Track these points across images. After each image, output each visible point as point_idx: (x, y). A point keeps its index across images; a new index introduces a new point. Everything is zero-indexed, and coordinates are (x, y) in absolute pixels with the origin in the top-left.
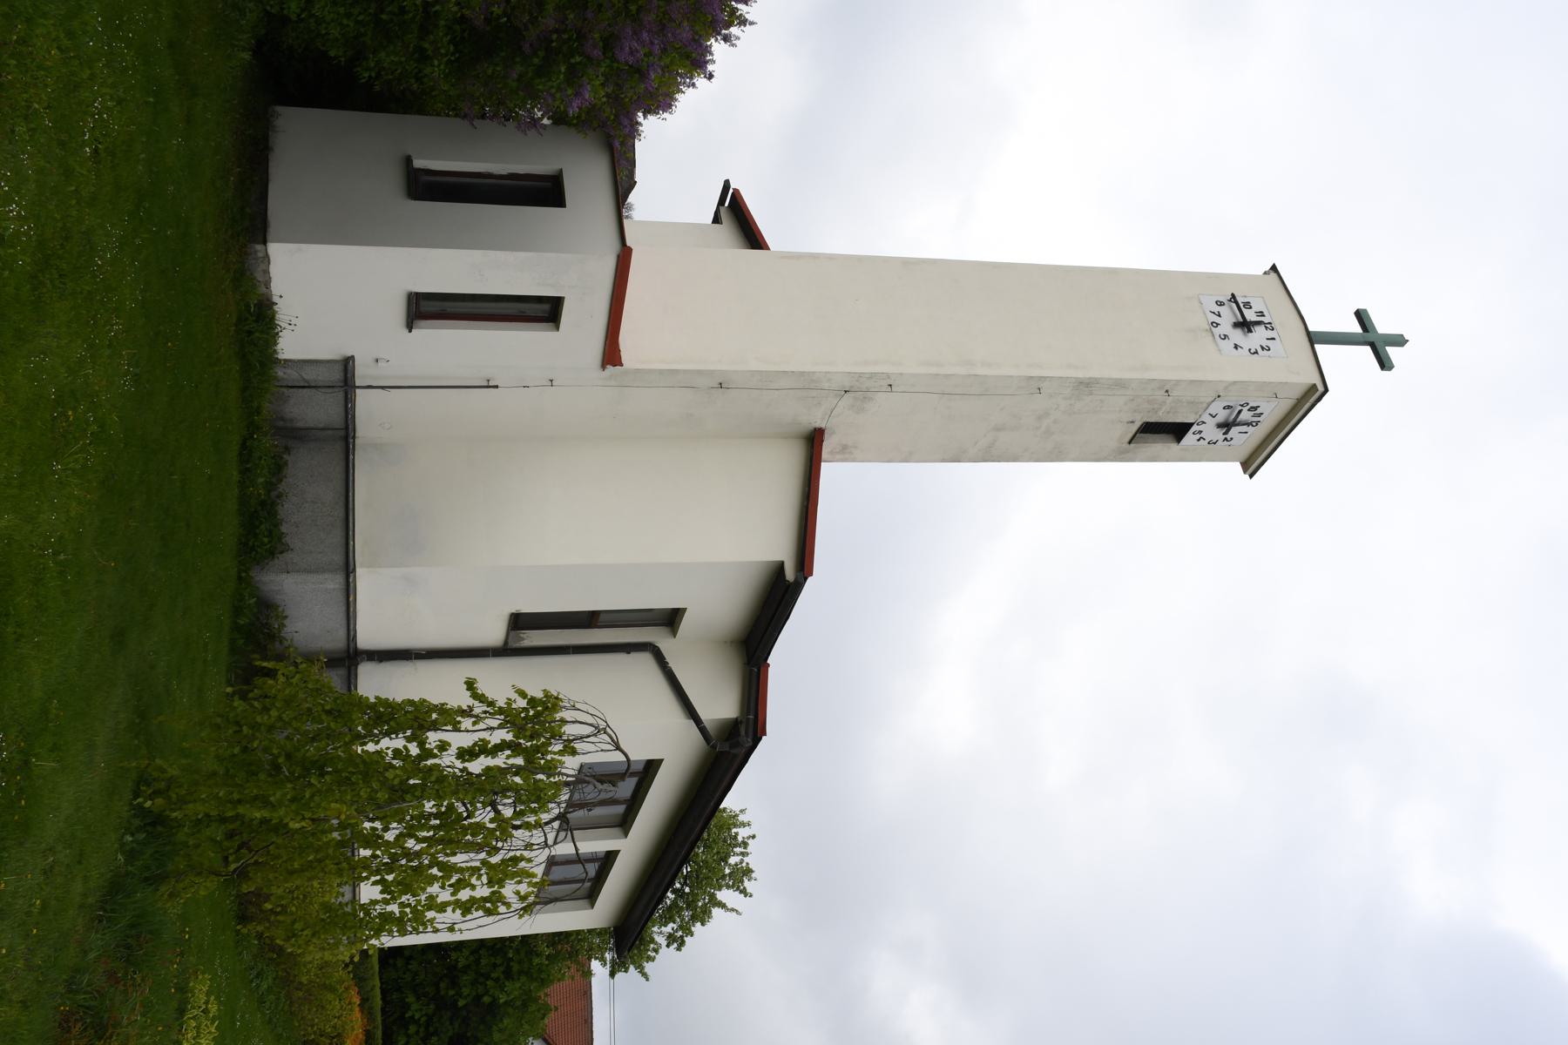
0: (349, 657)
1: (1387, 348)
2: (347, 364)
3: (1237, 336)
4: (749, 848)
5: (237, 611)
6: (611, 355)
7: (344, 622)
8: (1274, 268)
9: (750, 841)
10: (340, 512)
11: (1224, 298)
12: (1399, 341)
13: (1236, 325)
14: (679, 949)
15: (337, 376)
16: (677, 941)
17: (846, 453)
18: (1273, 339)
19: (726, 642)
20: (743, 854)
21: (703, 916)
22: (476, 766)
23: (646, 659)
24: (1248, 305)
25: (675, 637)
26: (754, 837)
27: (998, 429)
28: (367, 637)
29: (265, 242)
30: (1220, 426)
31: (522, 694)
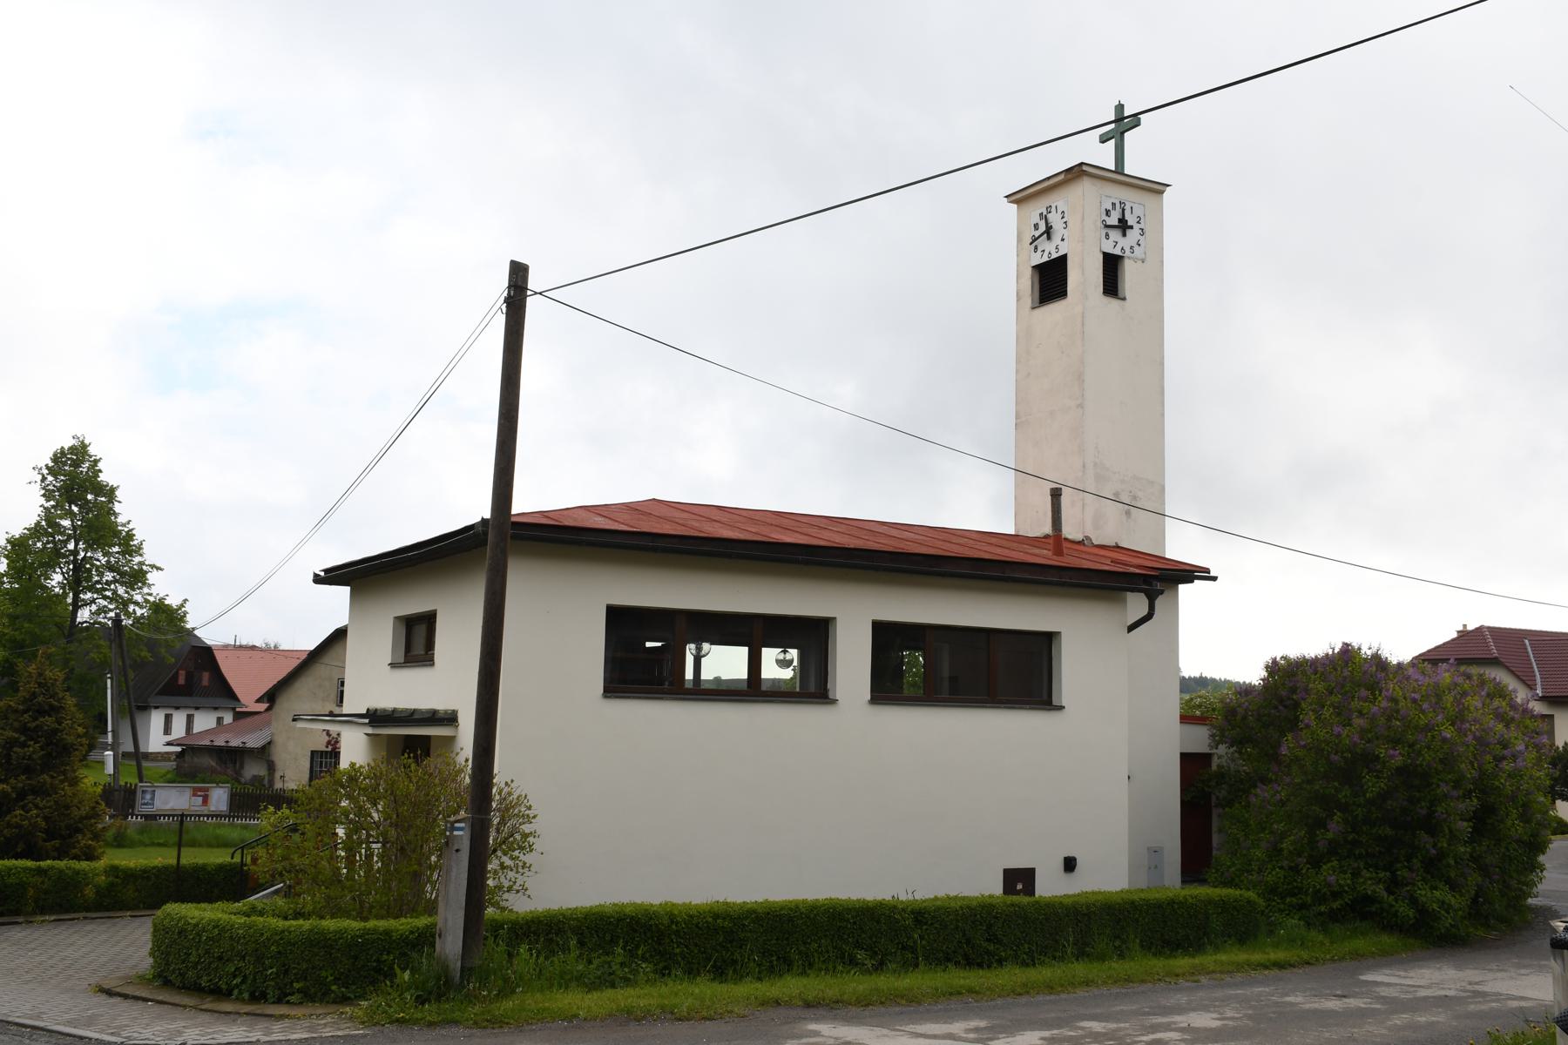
13: (1049, 238)
30: (1124, 235)
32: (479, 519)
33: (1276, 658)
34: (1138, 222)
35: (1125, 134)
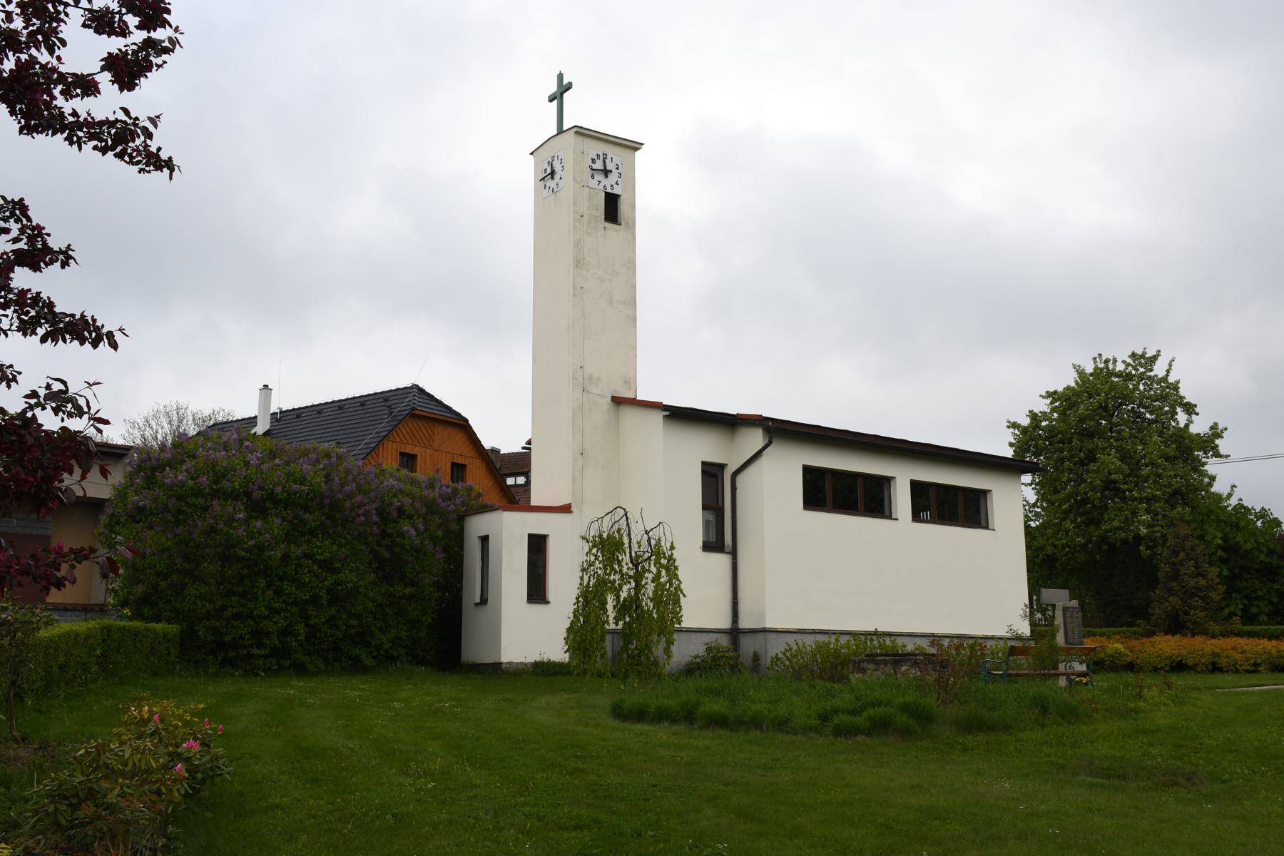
1: (564, 84)
3: (557, 177)
6: (566, 509)
7: (705, 634)
8: (532, 154)
12: (560, 76)
13: (552, 178)
17: (631, 382)
23: (739, 478)
27: (611, 302)
29: (501, 663)
30: (606, 177)
32: (874, 630)
33: (12, 281)
34: (617, 168)
35: (564, 95)
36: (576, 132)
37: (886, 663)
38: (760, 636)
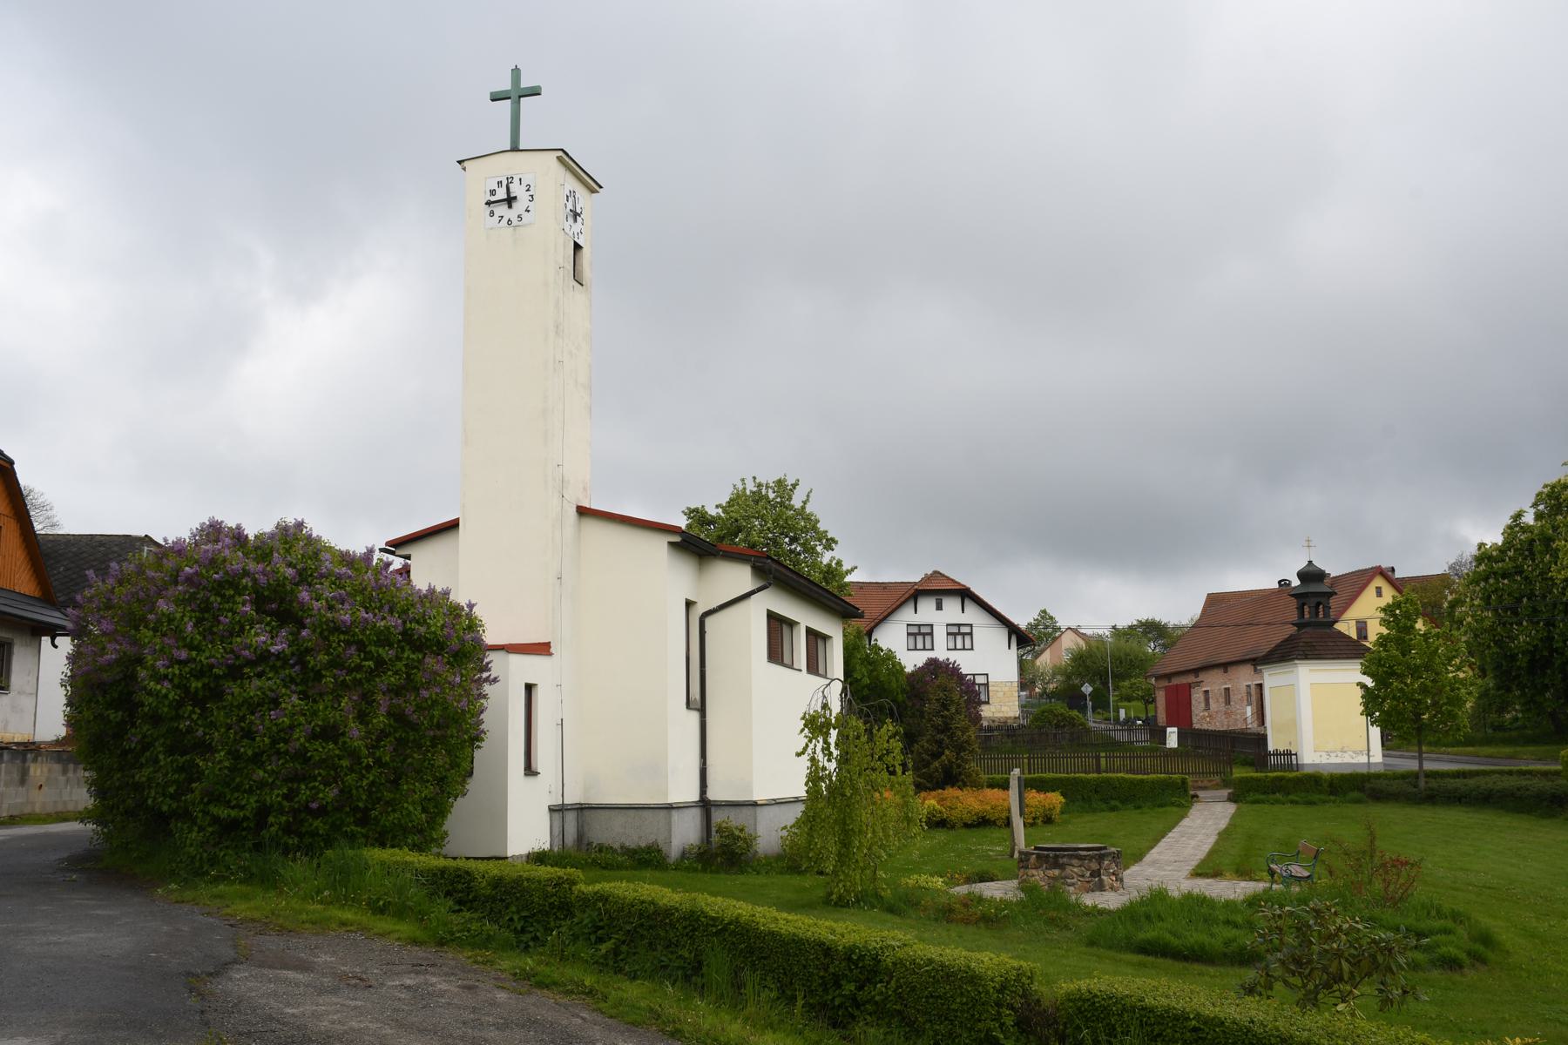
0: (703, 806)
2: (552, 810)
3: (519, 207)
4: (762, 482)
5: (695, 870)
9: (757, 481)
10: (632, 812)
11: (488, 210)
14: (836, 543)
15: (557, 816)
16: (830, 544)
18: (520, 179)
19: (700, 569)
20: (767, 487)
21: (812, 523)
22: (835, 753)
23: (709, 621)
24: (493, 192)
25: (696, 602)
26: (754, 478)
28: (694, 796)
31: (802, 731)
34: (528, 190)
36: (559, 158)
37: (1091, 858)
38: (745, 810)
